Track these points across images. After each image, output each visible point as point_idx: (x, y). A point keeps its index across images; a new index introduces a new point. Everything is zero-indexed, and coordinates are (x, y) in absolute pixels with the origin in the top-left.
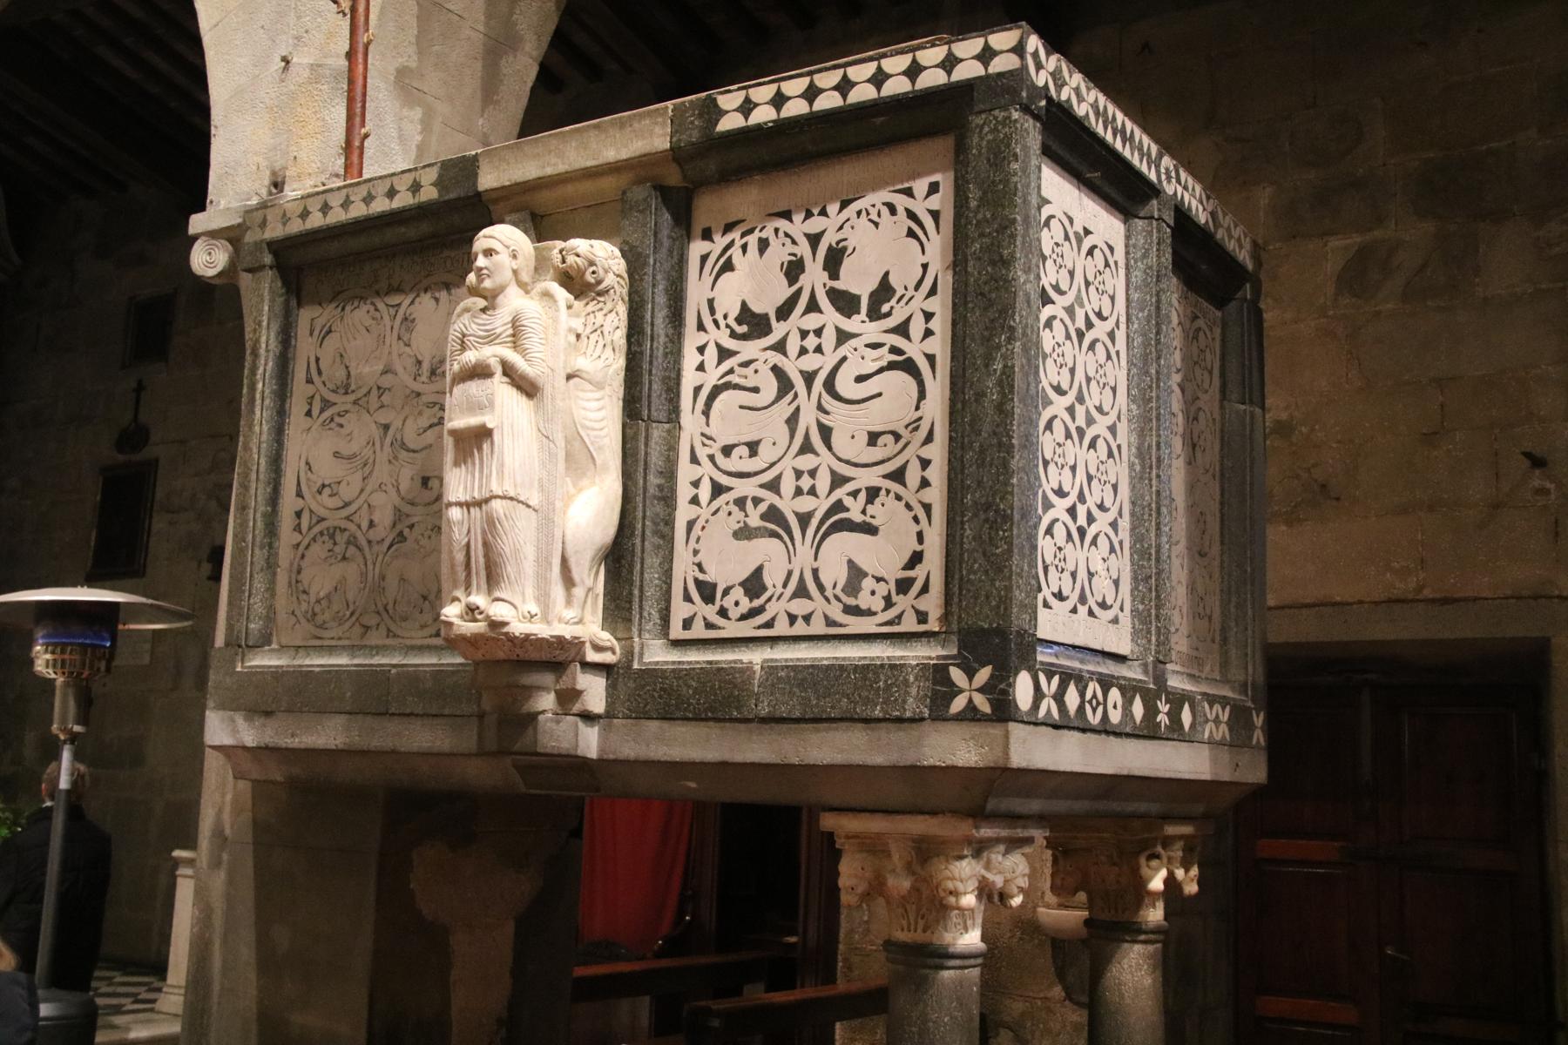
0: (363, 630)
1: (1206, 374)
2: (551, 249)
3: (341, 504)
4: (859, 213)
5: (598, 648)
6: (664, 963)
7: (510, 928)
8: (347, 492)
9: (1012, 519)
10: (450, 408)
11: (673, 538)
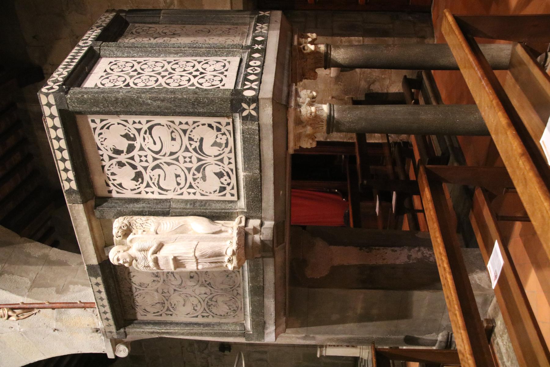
0: (238, 295)
1: (150, 29)
2: (116, 240)
3: (199, 303)
4: (102, 144)
5: (241, 222)
6: (349, 198)
7: (332, 247)
8: (196, 302)
9: (197, 97)
10: (168, 270)
11: (206, 200)
